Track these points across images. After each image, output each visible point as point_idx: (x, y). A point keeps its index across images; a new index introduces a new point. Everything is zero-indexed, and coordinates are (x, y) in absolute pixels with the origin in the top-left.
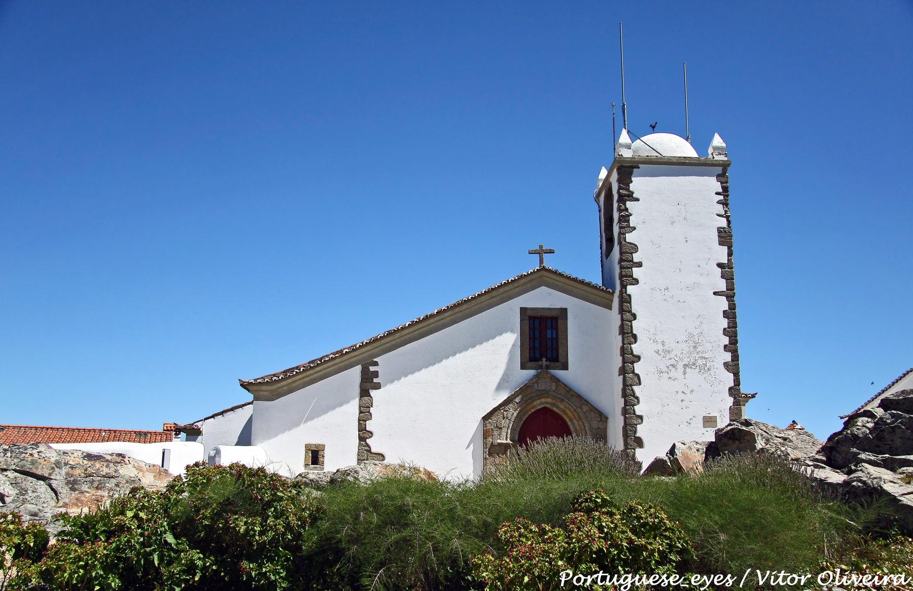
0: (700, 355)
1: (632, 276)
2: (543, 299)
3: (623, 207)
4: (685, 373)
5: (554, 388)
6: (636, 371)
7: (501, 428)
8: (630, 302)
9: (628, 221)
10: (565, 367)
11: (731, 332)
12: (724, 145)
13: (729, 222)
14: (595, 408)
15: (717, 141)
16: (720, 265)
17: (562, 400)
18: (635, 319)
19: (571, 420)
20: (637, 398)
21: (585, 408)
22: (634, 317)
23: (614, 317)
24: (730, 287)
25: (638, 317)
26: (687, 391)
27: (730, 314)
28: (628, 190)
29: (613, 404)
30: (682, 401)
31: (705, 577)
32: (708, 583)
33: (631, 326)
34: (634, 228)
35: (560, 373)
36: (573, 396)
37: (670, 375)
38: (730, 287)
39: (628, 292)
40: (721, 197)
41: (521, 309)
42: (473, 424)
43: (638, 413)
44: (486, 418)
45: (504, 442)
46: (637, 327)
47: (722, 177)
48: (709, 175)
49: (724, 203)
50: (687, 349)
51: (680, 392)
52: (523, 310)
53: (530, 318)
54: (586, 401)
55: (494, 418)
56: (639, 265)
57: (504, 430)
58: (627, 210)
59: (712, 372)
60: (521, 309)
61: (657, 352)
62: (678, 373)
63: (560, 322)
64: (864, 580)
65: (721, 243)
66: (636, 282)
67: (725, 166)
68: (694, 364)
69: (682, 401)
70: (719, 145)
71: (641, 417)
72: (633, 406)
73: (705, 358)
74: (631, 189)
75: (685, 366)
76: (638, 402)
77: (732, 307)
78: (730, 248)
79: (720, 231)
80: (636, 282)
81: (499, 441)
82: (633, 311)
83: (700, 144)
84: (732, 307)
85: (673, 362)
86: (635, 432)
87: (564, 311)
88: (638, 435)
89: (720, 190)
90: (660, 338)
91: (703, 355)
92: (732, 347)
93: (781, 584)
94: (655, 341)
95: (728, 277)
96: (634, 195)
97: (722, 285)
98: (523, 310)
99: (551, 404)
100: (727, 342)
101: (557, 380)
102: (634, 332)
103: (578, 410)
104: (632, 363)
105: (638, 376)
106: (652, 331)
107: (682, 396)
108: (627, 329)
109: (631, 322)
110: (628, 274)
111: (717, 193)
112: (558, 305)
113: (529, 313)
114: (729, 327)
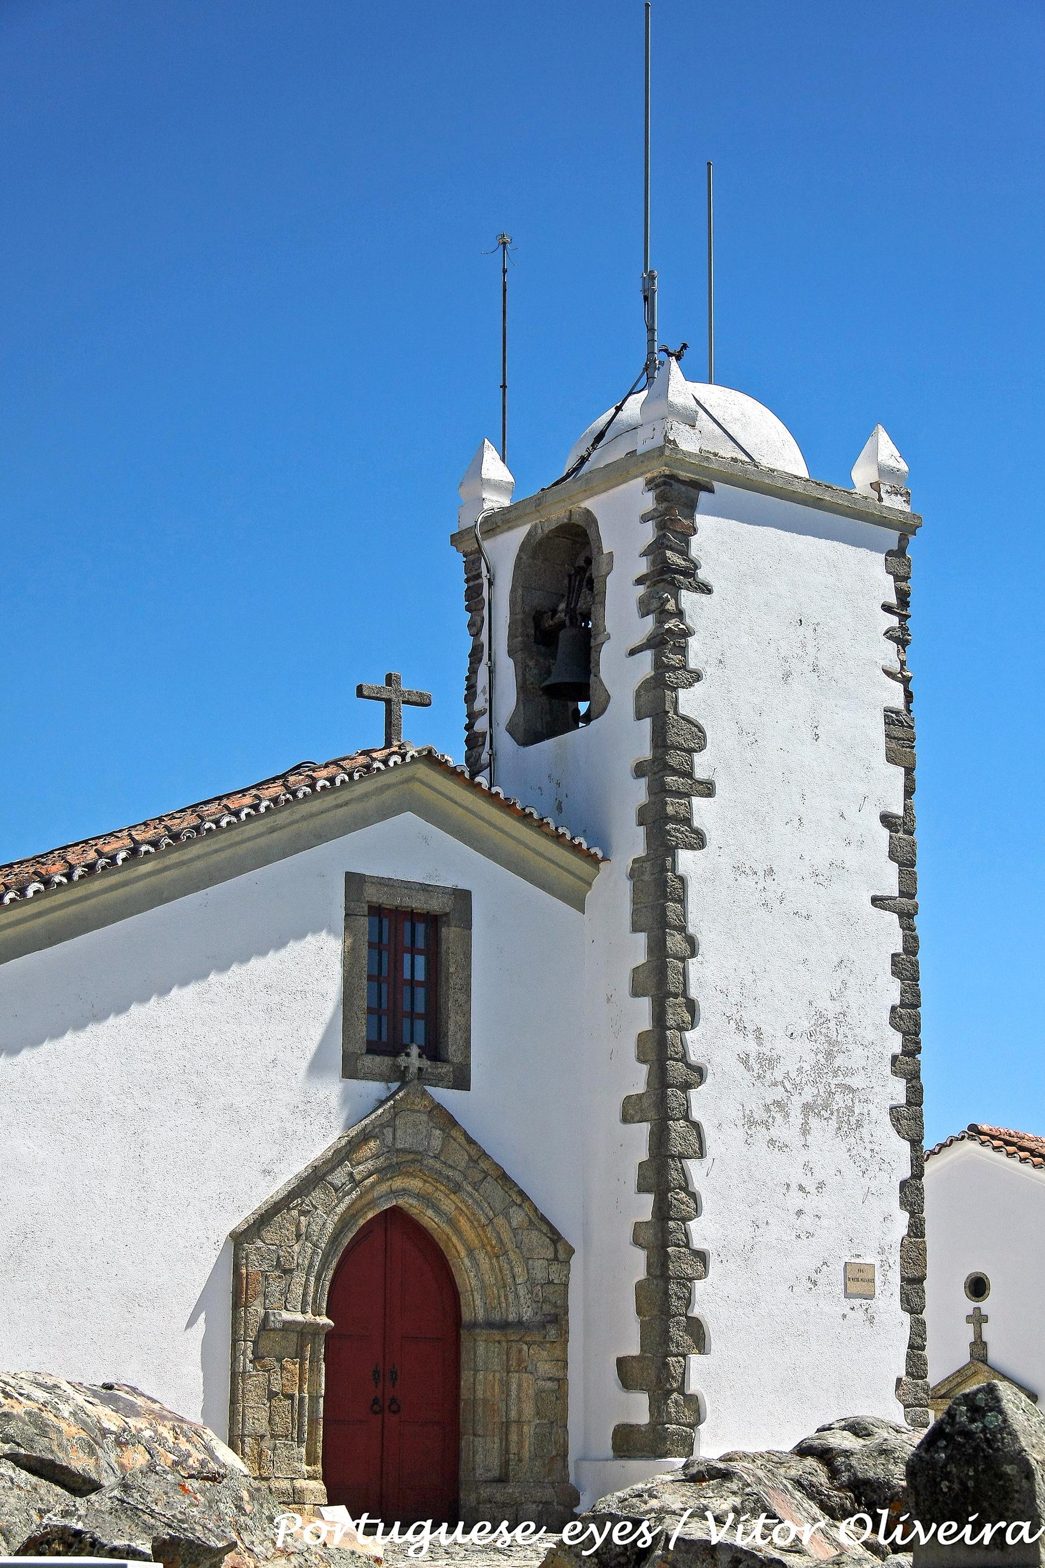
0: (840, 1079)
1: (687, 821)
2: (412, 853)
3: (671, 606)
4: (805, 1131)
5: (436, 1143)
6: (696, 1115)
7: (287, 1272)
8: (682, 901)
9: (683, 650)
10: (462, 1082)
11: (907, 1017)
12: (903, 467)
13: (909, 696)
14: (543, 1218)
15: (885, 449)
16: (887, 820)
17: (457, 1189)
18: (694, 954)
19: (470, 1252)
20: (693, 1196)
21: (518, 1217)
22: (692, 944)
23: (608, 929)
24: (908, 892)
25: (702, 949)
26: (810, 1186)
27: (905, 967)
28: (684, 553)
29: (600, 1207)
30: (800, 1213)
31: (593, 1528)
32: (599, 1541)
33: (685, 974)
34: (697, 677)
35: (443, 1095)
36: (486, 1174)
37: (774, 1132)
38: (908, 892)
39: (681, 870)
40: (894, 621)
41: (347, 873)
42: (195, 1260)
43: (697, 1244)
44: (239, 1239)
45: (299, 1317)
46: (703, 976)
47: (897, 558)
48: (873, 547)
49: (900, 639)
50: (810, 1059)
51: (794, 1187)
52: (354, 881)
53: (376, 911)
54: (521, 1193)
55: (270, 1234)
56: (708, 789)
57: (299, 1278)
58: (680, 614)
59: (865, 1131)
60: (347, 873)
61: (745, 1061)
62: (787, 1131)
63: (449, 934)
64: (616, 1534)
65: (891, 759)
66: (698, 841)
67: (907, 529)
68: (825, 1108)
69: (800, 1213)
70: (892, 463)
71: (702, 1257)
72: (685, 1220)
73: (850, 1089)
74: (694, 553)
75: (807, 1108)
76: (698, 1211)
77: (911, 945)
78: (909, 771)
79: (892, 719)
80: (698, 841)
81: (286, 1316)
82: (691, 930)
83: (829, 441)
84: (911, 945)
85: (779, 1093)
86: (689, 1302)
87: (463, 897)
88: (696, 1312)
89: (893, 600)
90: (752, 1016)
91: (848, 1081)
92: (907, 1064)
93: (1028, 1540)
94: (741, 1028)
95: (905, 860)
96: (702, 574)
97: (888, 880)
98: (354, 881)
99: (418, 1196)
100: (898, 1049)
101: (447, 1121)
102: (693, 993)
103: (500, 1221)
104: (686, 1086)
105: (696, 1126)
106: (734, 992)
107: (796, 1200)
108: (673, 983)
109: (683, 959)
110: (682, 811)
111: (887, 608)
112: (449, 881)
113: (372, 894)
114: (903, 1005)
